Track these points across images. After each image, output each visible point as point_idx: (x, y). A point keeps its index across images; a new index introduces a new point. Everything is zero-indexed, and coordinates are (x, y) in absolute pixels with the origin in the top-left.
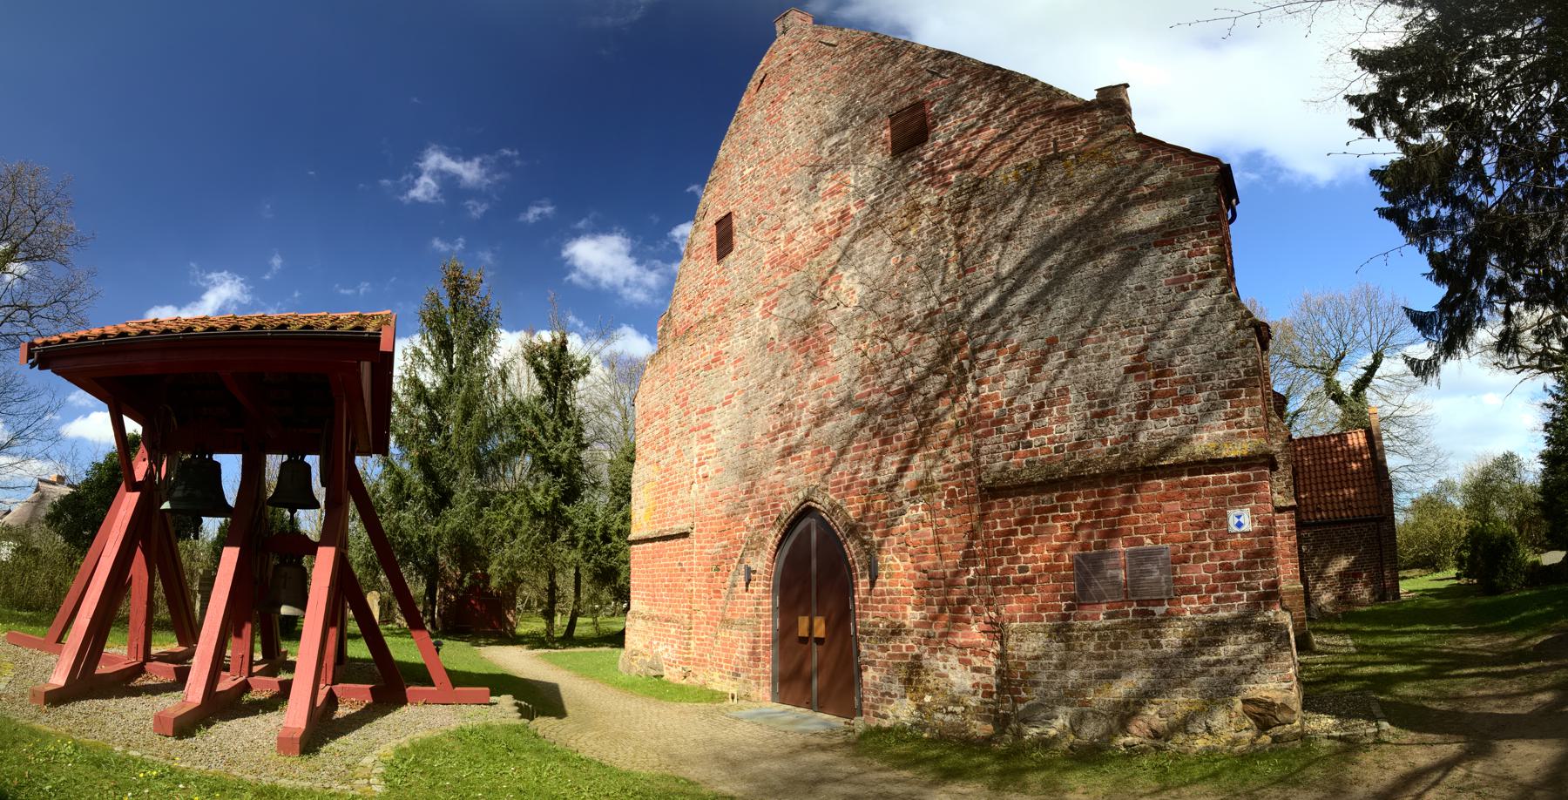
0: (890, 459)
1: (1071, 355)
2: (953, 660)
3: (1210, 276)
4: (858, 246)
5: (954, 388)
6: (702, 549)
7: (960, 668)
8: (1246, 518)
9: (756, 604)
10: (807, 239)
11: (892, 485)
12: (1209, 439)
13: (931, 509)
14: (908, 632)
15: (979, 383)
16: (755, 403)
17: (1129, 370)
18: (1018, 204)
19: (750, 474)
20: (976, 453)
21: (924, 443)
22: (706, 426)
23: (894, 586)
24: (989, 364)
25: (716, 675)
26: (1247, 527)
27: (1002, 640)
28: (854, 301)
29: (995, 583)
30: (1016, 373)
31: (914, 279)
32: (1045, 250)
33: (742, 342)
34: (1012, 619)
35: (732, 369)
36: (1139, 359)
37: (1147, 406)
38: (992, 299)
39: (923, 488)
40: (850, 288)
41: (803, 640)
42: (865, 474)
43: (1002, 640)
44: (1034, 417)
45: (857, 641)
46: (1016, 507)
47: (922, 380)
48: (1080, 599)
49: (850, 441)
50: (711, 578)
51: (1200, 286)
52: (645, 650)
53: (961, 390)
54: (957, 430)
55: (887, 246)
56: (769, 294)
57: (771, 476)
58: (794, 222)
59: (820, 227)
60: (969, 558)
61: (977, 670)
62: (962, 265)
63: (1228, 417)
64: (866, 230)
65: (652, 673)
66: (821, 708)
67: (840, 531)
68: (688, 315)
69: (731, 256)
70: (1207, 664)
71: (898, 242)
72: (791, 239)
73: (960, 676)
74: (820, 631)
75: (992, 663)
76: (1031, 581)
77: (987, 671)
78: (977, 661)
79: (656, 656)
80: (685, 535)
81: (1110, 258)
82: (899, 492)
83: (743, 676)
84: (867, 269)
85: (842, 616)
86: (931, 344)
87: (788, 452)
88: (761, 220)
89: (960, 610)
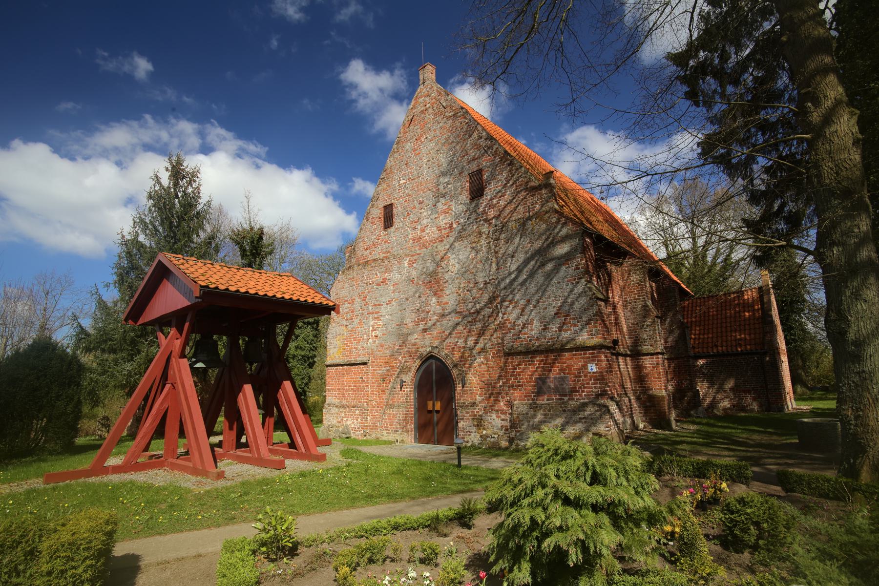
0: (470, 339)
1: (535, 307)
2: (494, 416)
3: (581, 278)
4: (456, 244)
5: (495, 313)
6: (372, 372)
7: (496, 419)
8: (594, 367)
9: (407, 396)
10: (431, 233)
11: (471, 349)
12: (584, 338)
13: (486, 359)
14: (477, 406)
15: (504, 314)
16: (404, 306)
17: (556, 314)
18: (517, 240)
19: (404, 339)
20: (503, 339)
21: (483, 334)
22: (377, 313)
23: (472, 386)
24: (507, 307)
25: (385, 432)
26: (594, 370)
27: (512, 408)
28: (455, 270)
29: (509, 386)
30: (517, 311)
31: (480, 266)
32: (526, 262)
33: (397, 276)
34: (515, 400)
35: (392, 288)
36: (559, 310)
37: (562, 327)
38: (507, 281)
39: (483, 350)
40: (454, 264)
41: (430, 412)
42: (461, 343)
43: (512, 408)
44: (522, 328)
45: (456, 410)
46: (516, 360)
47: (482, 309)
48: (539, 392)
49: (453, 329)
50: (379, 385)
51: (578, 283)
52: (337, 424)
53: (497, 315)
54: (496, 330)
55: (469, 249)
56: (412, 256)
57: (414, 338)
58: (425, 222)
59: (440, 229)
60: (500, 377)
61: (503, 420)
62: (497, 265)
63: (588, 332)
64: (459, 238)
65: (344, 436)
66: (439, 442)
67: (450, 366)
68: (366, 253)
69: (392, 229)
70: (580, 418)
71: (473, 248)
72: (423, 231)
73: (496, 422)
74: (438, 406)
75: (508, 417)
76: (522, 386)
77: (506, 420)
78: (503, 417)
79: (347, 426)
80: (365, 364)
81: (549, 266)
82: (474, 352)
83: (400, 431)
84: (461, 257)
85: (449, 401)
86: (486, 297)
87: (425, 330)
88: (408, 214)
89: (498, 397)
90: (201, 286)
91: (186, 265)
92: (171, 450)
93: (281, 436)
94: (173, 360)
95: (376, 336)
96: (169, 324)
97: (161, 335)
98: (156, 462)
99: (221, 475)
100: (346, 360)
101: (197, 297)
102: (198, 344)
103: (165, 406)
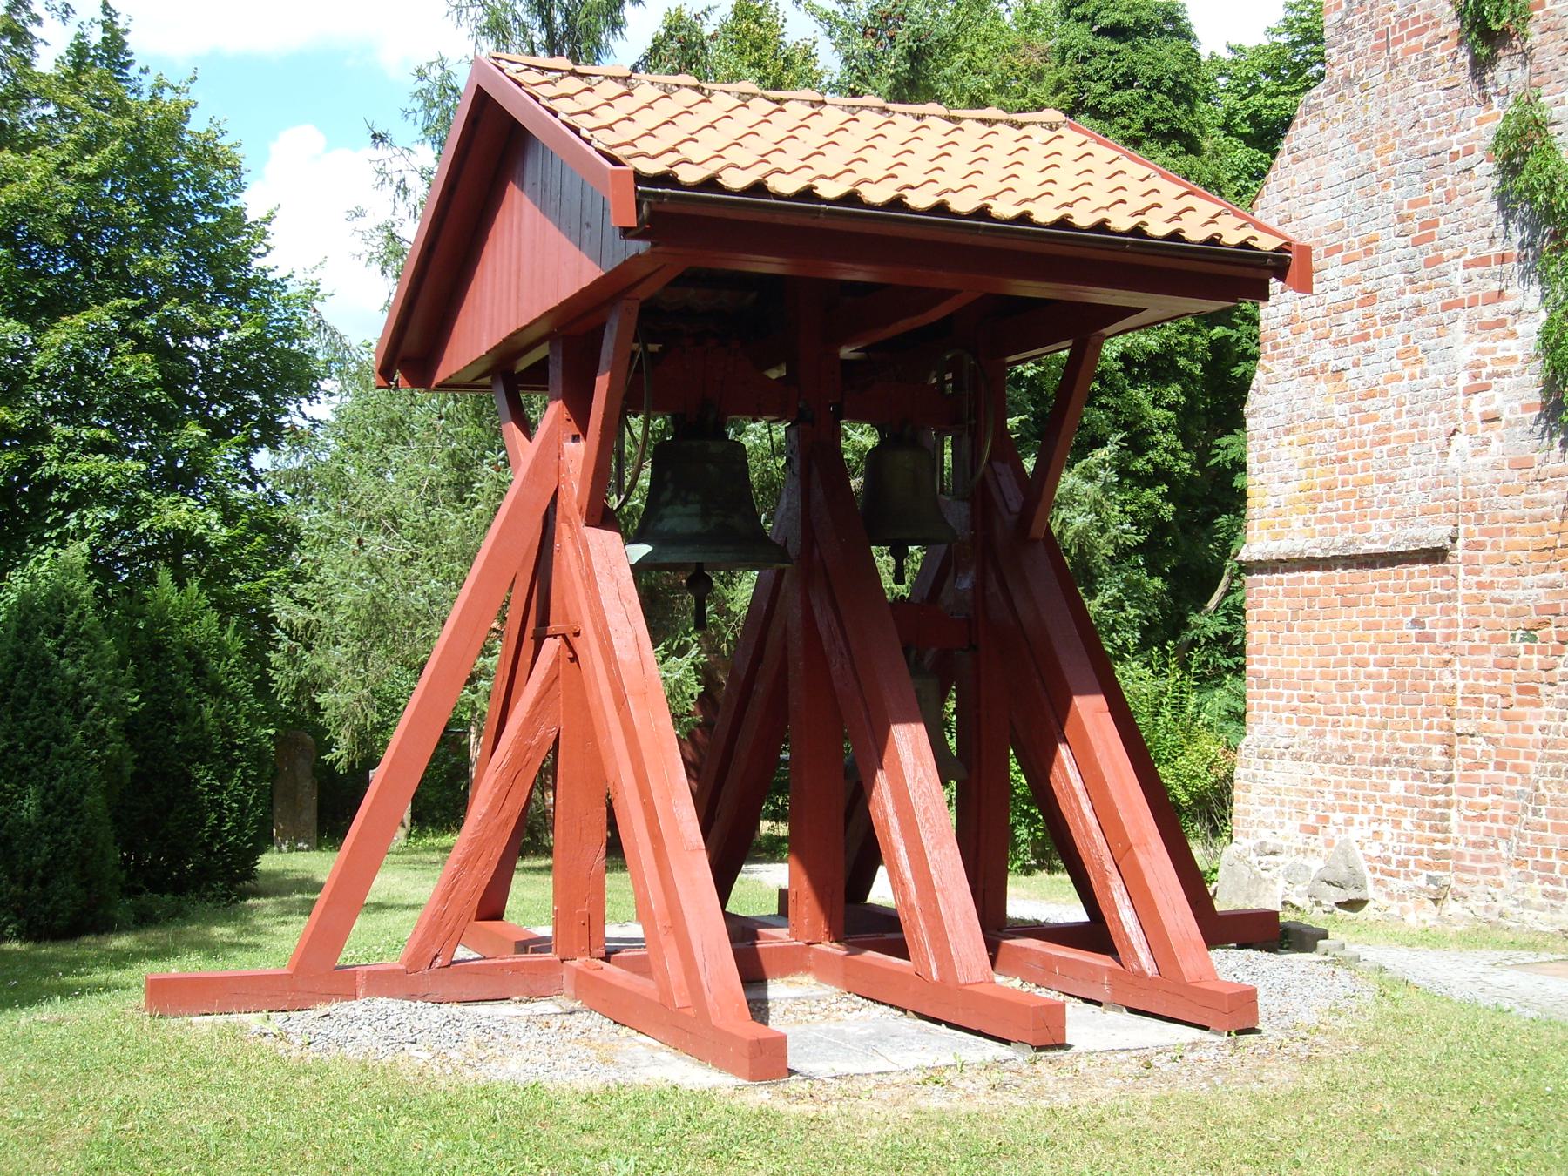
80: (1435, 555)
90: (639, 178)
91: (588, 100)
92: (581, 914)
93: (1041, 897)
94: (563, 532)
95: (1490, 419)
96: (537, 378)
97: (1069, 534)
98: (528, 970)
99: (768, 1061)
100: (1335, 544)
101: (626, 232)
102: (663, 457)
103: (546, 733)
